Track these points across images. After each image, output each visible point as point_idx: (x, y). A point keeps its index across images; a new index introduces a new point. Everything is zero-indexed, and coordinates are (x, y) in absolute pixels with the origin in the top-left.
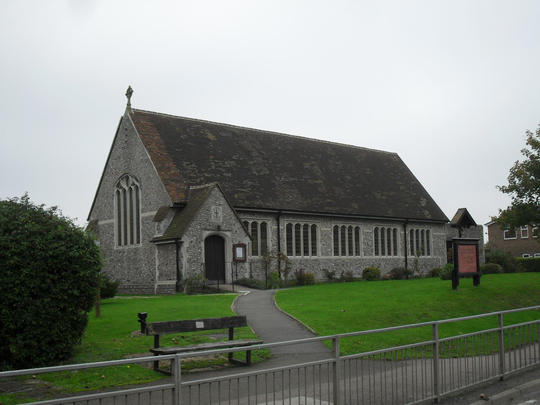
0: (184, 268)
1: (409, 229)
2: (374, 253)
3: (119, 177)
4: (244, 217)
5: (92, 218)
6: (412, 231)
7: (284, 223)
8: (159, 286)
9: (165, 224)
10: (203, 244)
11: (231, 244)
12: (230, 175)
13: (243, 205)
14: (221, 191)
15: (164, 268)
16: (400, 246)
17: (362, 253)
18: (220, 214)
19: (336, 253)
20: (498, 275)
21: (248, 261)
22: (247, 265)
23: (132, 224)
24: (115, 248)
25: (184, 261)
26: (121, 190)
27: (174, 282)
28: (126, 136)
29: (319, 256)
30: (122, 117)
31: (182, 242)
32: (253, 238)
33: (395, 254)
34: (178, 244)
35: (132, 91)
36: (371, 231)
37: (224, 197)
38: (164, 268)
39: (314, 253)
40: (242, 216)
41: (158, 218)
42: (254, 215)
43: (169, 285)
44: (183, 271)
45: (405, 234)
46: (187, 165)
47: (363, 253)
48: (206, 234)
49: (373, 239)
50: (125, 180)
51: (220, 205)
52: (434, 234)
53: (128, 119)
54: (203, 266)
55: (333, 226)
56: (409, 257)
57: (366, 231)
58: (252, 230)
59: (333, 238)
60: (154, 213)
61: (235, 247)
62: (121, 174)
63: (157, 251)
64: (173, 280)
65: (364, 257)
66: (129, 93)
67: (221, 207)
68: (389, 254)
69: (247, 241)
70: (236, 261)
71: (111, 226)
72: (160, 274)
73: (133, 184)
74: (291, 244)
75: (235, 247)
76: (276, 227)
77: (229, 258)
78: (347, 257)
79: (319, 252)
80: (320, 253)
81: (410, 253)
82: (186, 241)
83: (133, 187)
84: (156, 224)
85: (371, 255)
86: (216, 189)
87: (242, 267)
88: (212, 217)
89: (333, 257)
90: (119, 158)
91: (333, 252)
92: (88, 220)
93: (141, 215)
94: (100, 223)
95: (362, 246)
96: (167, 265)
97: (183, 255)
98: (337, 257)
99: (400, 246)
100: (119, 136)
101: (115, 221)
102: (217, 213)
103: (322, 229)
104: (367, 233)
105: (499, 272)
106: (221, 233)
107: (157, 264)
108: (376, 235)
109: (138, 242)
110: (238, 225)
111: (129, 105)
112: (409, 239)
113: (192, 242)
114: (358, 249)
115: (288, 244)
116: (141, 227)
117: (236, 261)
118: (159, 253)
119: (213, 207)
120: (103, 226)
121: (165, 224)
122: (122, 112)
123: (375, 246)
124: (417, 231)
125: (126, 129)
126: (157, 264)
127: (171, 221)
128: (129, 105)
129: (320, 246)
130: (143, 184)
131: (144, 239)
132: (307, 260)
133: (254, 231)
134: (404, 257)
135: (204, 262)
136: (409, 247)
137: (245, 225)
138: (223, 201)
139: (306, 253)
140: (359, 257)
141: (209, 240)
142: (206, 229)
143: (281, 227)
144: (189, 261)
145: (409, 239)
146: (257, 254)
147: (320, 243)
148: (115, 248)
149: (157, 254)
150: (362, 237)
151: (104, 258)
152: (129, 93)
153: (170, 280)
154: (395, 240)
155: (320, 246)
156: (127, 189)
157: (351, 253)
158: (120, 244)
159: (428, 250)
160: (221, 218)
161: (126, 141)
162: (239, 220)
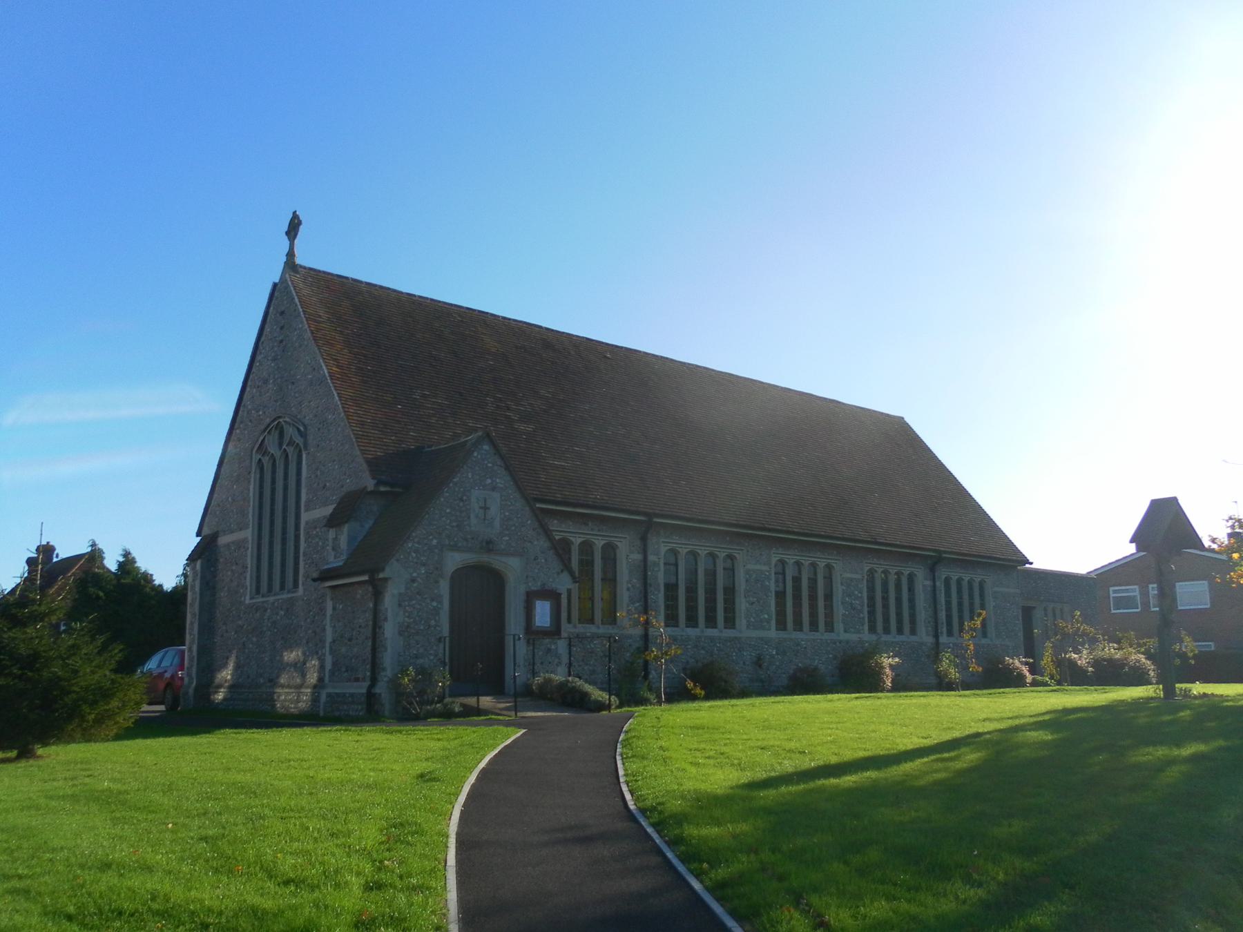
0: (389, 650)
1: (943, 573)
2: (866, 627)
3: (263, 427)
4: (560, 529)
5: (206, 531)
6: (947, 581)
7: (660, 547)
8: (329, 695)
9: (343, 537)
10: (444, 587)
11: (522, 589)
12: (530, 428)
13: (559, 497)
14: (497, 451)
15: (343, 650)
16: (923, 614)
17: (839, 626)
18: (494, 510)
19: (781, 625)
20: (696, 705)
21: (564, 634)
22: (561, 646)
23: (284, 541)
24: (247, 602)
25: (389, 630)
26: (265, 460)
27: (361, 688)
28: (282, 328)
29: (743, 629)
30: (275, 285)
31: (127, 563)
32: (584, 575)
33: (913, 631)
34: (377, 589)
35: (300, 223)
36: (859, 576)
37: (507, 468)
38: (343, 650)
39: (730, 622)
40: (554, 525)
41: (333, 521)
42: (586, 524)
43: (352, 695)
44: (388, 660)
45: (934, 586)
46: (424, 396)
47: (841, 625)
48: (454, 561)
49: (865, 595)
50: (276, 434)
51: (494, 489)
52: (996, 589)
53: (287, 287)
54: (441, 645)
55: (774, 560)
56: (943, 639)
57: (849, 575)
58: (581, 562)
59: (773, 588)
60: (329, 510)
61: (530, 598)
62: (268, 420)
63: (329, 605)
64: (364, 680)
65: (844, 636)
66: (294, 227)
67: (496, 495)
68: (900, 631)
69: (563, 584)
70: (532, 633)
71: (240, 545)
72: (334, 664)
73: (291, 443)
74: (675, 599)
75: (530, 598)
76: (639, 557)
77: (514, 624)
78: (805, 637)
79: (741, 622)
80: (744, 622)
81: (945, 629)
82: (398, 576)
83: (290, 450)
84: (332, 533)
85: (859, 632)
86: (486, 447)
87: (549, 650)
88: (472, 516)
89: (772, 633)
90: (266, 382)
91: (773, 622)
92: (198, 535)
93: (305, 517)
94: (223, 540)
95: (839, 611)
96: (350, 640)
97: (389, 614)
98: (782, 635)
99: (923, 614)
100: (267, 329)
101: (248, 534)
102: (485, 508)
103: (750, 567)
104: (852, 580)
105: (1024, 685)
106: (496, 562)
107: (329, 639)
108: (871, 589)
109: (296, 585)
110: (543, 543)
111: (291, 254)
112: (942, 599)
113: (413, 581)
114: (829, 614)
115: (667, 598)
116: (303, 545)
117: (532, 633)
118: (334, 609)
119: (476, 494)
120: (228, 545)
121: (343, 537)
122: (274, 273)
123: (869, 612)
124: (959, 581)
125: (282, 313)
126: (329, 639)
127: (367, 526)
128: (291, 254)
129: (743, 608)
130: (310, 438)
131: (306, 577)
132: (712, 639)
133: (587, 564)
134: (930, 640)
135: (445, 630)
136: (942, 615)
137: (561, 549)
138: (502, 480)
139: (711, 621)
140: (833, 636)
141: (461, 576)
142: (455, 548)
143: (651, 558)
144: (404, 630)
145: (942, 599)
146: (801, 630)
147: (743, 600)
148: (247, 602)
149: (329, 611)
150: (839, 590)
151: (225, 624)
152: (294, 227)
153: (357, 680)
154: (912, 601)
155: (743, 608)
156: (278, 454)
157: (814, 626)
158: (258, 591)
159: (913, 621)
160: (497, 523)
161: (281, 341)
162: (548, 533)
